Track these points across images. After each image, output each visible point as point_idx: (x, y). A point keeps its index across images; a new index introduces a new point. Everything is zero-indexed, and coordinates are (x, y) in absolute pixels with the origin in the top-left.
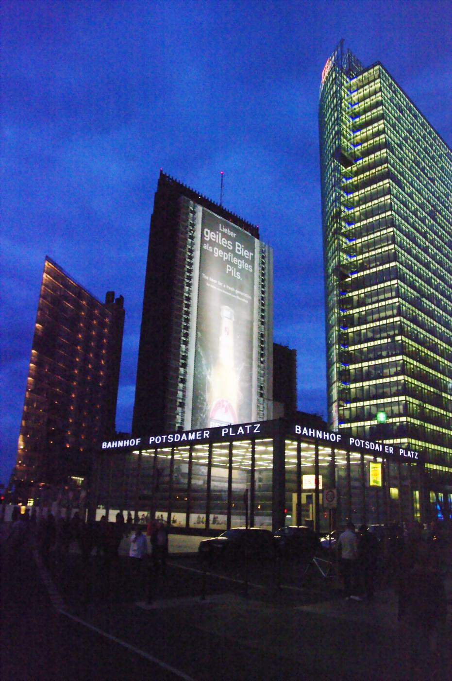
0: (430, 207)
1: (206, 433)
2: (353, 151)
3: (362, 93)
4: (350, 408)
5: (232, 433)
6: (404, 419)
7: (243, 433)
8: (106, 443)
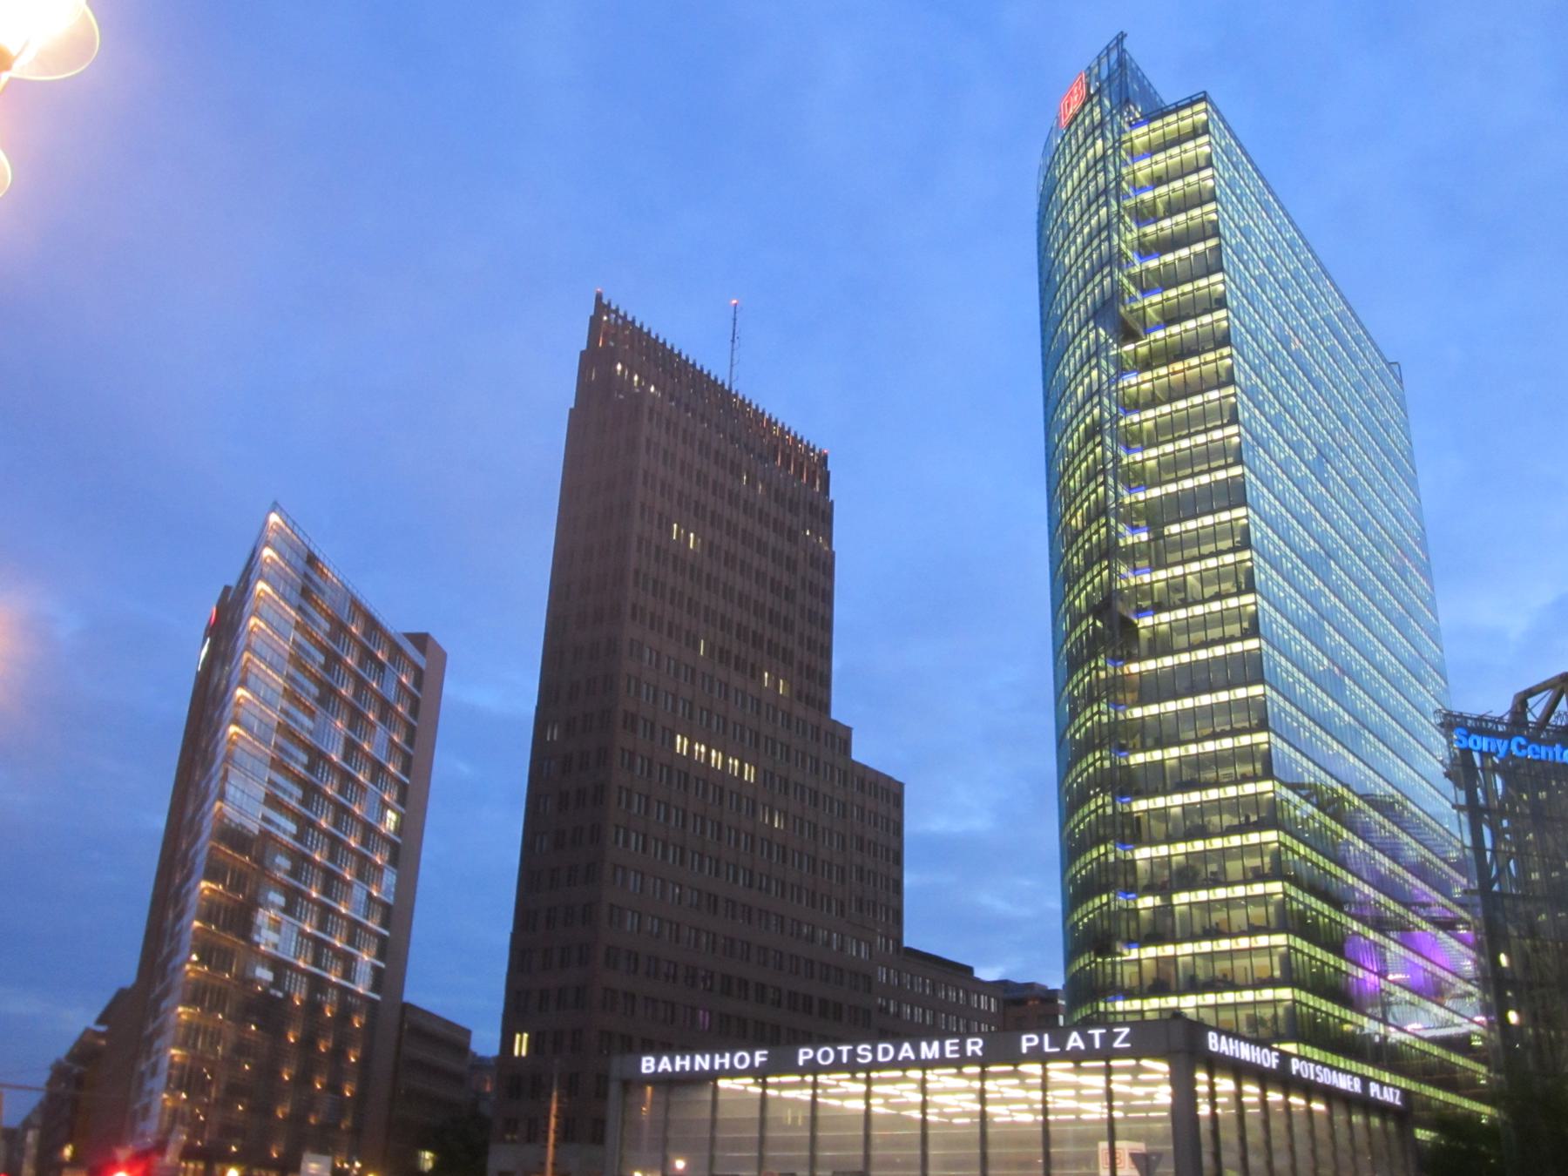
0: (1326, 662)
1: (974, 1044)
2: (1136, 306)
3: (1161, 162)
4: (1139, 961)
5: (1051, 1045)
6: (1285, 993)
7: (1082, 1047)
8: (652, 1059)
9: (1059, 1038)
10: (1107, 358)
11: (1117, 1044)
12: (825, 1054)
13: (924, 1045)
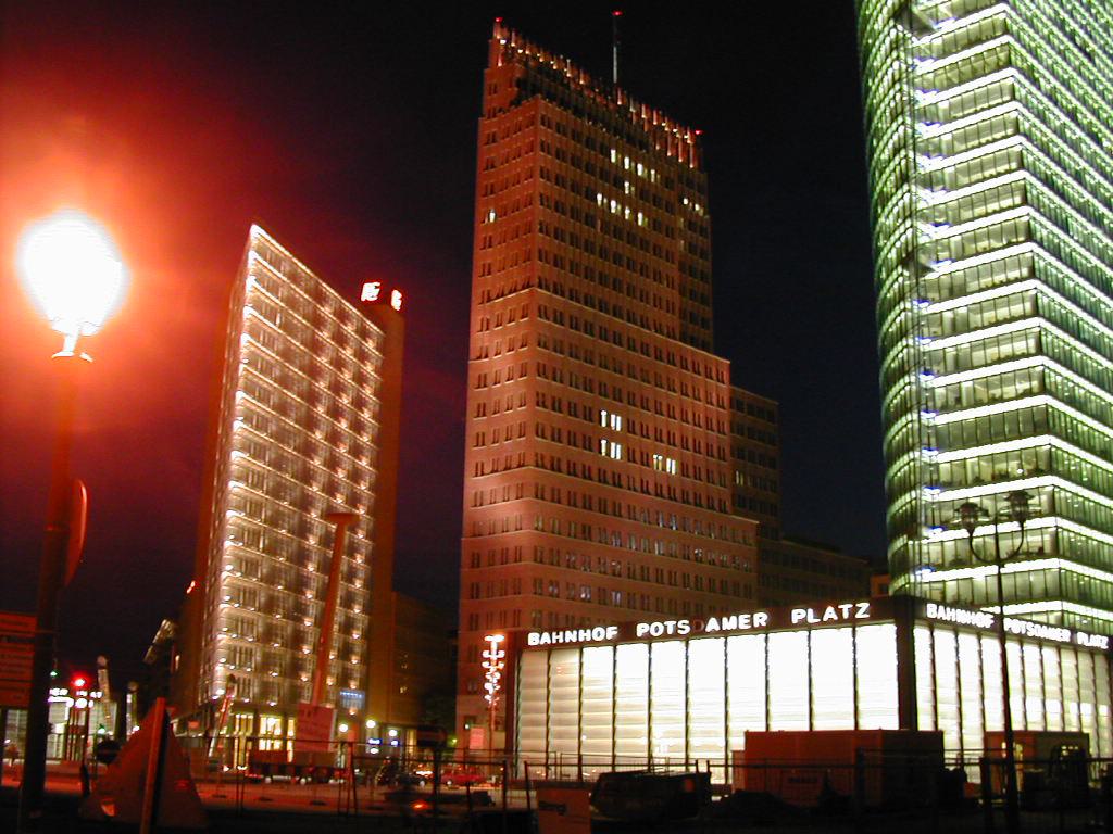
6: (1054, 563)
8: (537, 635)
9: (820, 613)
10: (905, 50)
11: (859, 615)
12: (656, 628)
13: (725, 620)
